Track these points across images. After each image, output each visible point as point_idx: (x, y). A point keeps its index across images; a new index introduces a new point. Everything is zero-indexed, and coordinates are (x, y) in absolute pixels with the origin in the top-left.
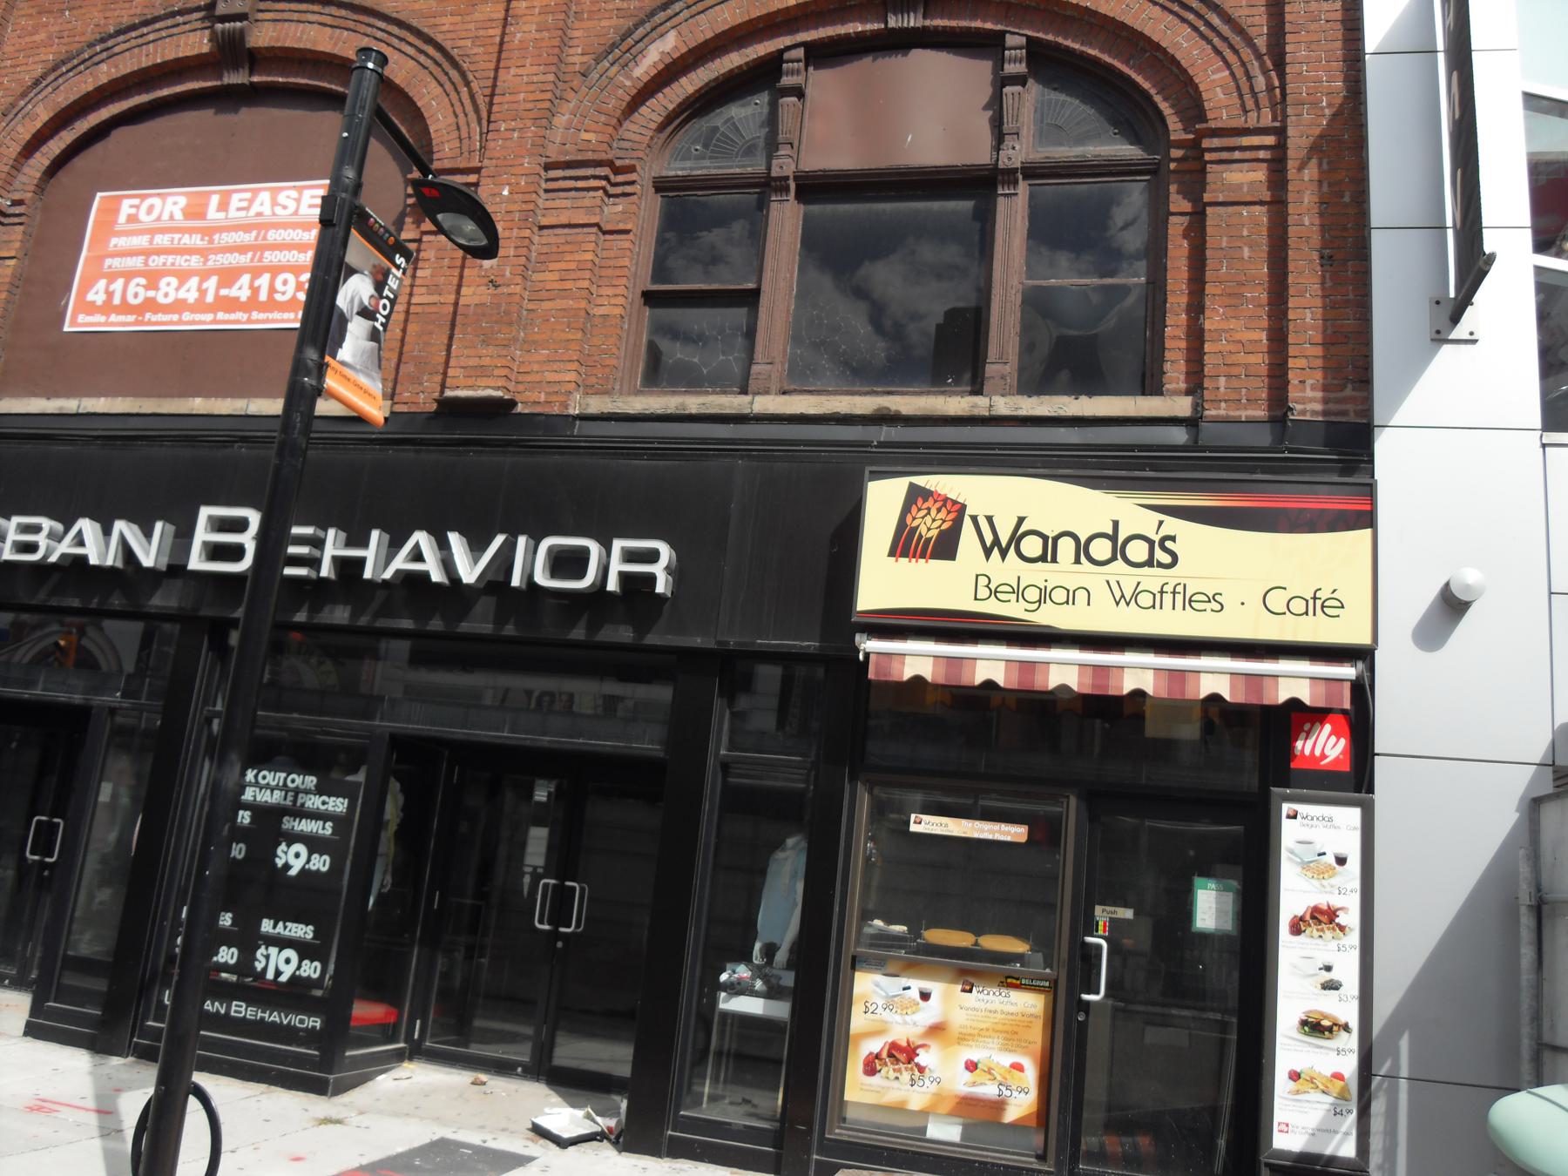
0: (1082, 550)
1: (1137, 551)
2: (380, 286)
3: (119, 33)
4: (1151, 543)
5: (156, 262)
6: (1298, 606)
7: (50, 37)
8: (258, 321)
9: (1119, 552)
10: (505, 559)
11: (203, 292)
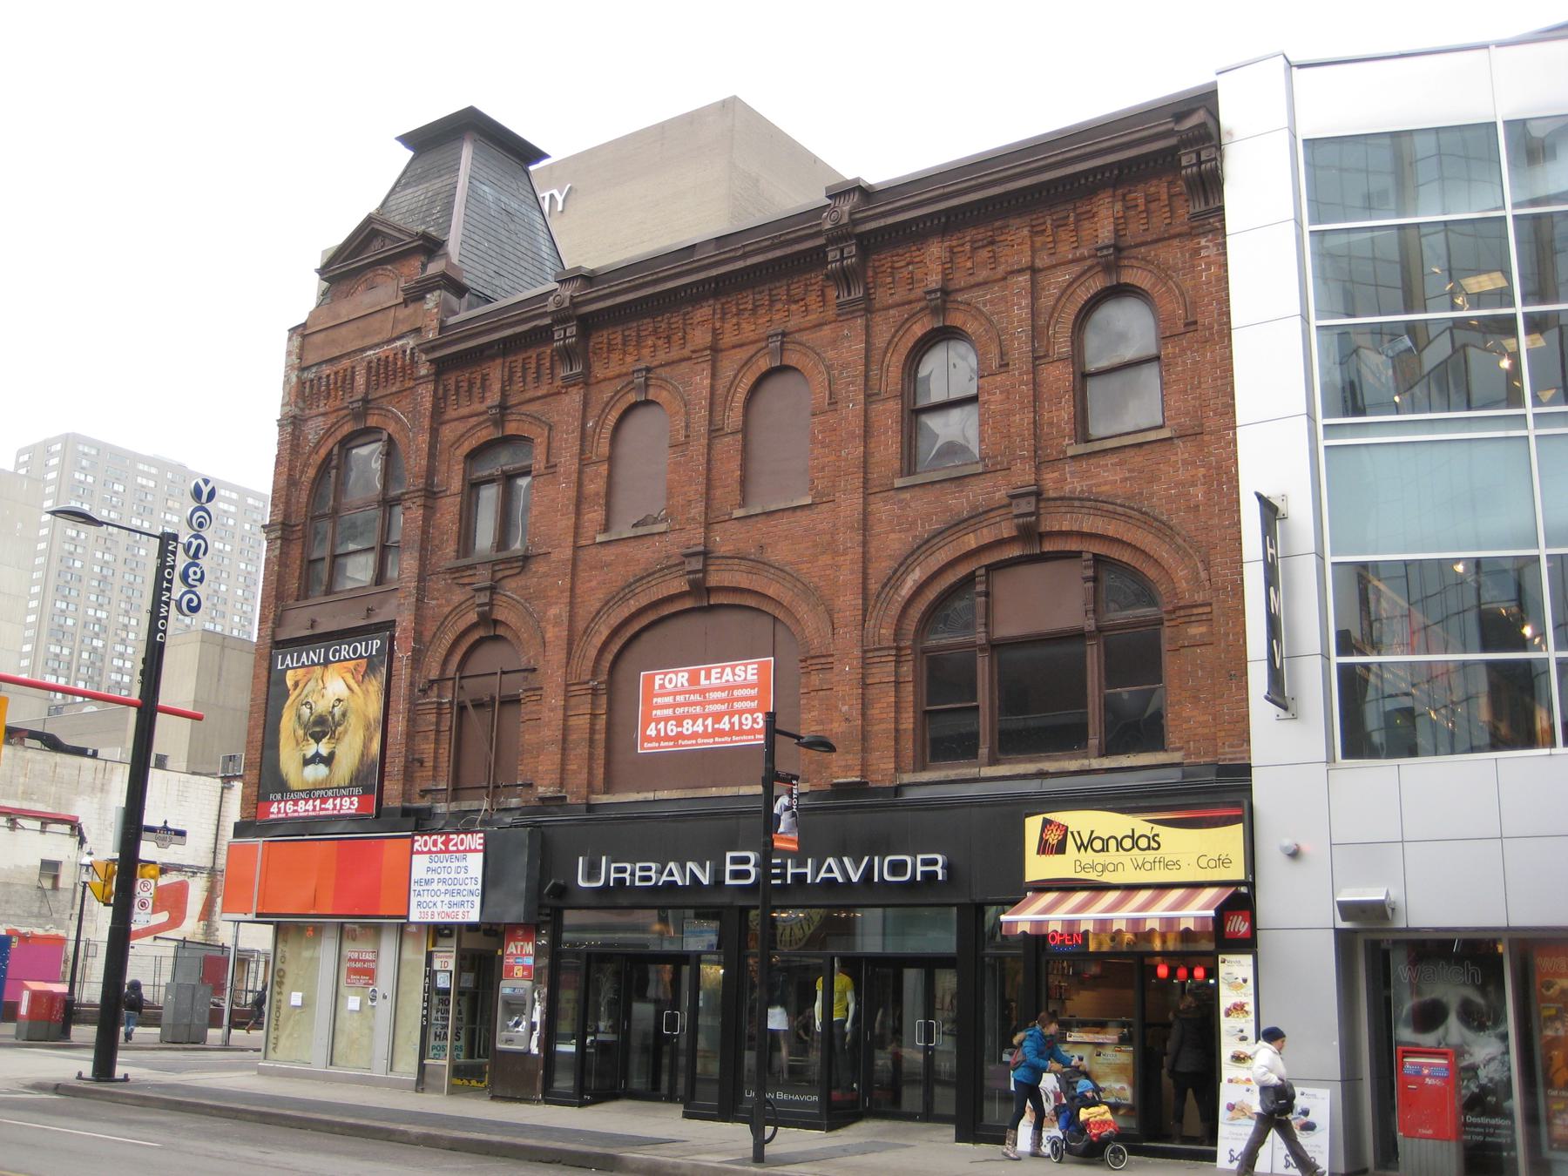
0: (1119, 844)
1: (1143, 843)
2: (791, 796)
3: (637, 581)
4: (1149, 838)
5: (679, 711)
6: (1212, 864)
7: (598, 584)
8: (736, 742)
9: (1135, 844)
10: (870, 867)
11: (706, 727)
